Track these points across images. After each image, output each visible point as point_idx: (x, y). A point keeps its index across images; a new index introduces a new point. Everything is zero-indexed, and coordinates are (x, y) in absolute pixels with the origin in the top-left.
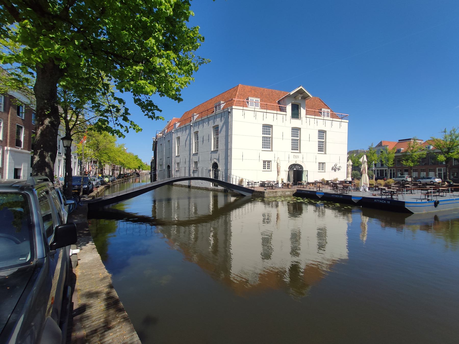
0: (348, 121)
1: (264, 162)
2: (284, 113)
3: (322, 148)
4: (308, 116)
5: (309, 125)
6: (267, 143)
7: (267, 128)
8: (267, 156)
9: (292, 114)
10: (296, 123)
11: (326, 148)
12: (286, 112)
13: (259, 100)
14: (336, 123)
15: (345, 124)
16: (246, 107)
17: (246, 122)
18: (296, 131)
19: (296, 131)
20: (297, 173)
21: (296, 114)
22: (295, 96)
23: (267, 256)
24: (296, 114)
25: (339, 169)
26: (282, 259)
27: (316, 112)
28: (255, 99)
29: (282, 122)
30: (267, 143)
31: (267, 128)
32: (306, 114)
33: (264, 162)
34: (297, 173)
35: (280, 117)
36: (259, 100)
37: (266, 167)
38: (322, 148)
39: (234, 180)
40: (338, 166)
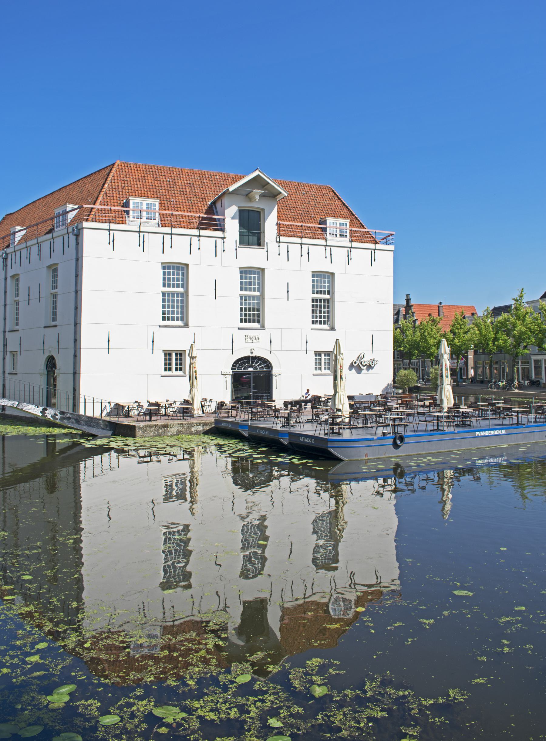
0: (392, 248)
1: (168, 354)
2: (220, 234)
3: (323, 311)
4: (282, 239)
5: (288, 264)
6: (176, 309)
7: (176, 273)
8: (176, 339)
9: (241, 235)
10: (252, 256)
11: (330, 315)
12: (223, 230)
13: (156, 202)
14: (362, 253)
15: (385, 257)
16: (124, 223)
17: (120, 267)
18: (253, 277)
19: (253, 277)
20: (252, 379)
21: (251, 231)
22: (245, 192)
23: (176, 577)
24: (251, 231)
25: (369, 367)
26: (218, 590)
27: (306, 224)
28: (144, 202)
29: (215, 261)
30: (176, 309)
31: (176, 273)
32: (279, 235)
33: (168, 354)
34: (252, 379)
35: (208, 244)
36: (156, 202)
37: (174, 367)
38: (323, 311)
39: (89, 406)
40: (367, 360)
